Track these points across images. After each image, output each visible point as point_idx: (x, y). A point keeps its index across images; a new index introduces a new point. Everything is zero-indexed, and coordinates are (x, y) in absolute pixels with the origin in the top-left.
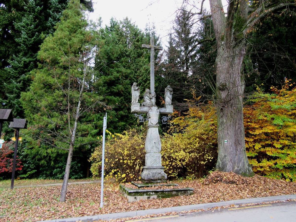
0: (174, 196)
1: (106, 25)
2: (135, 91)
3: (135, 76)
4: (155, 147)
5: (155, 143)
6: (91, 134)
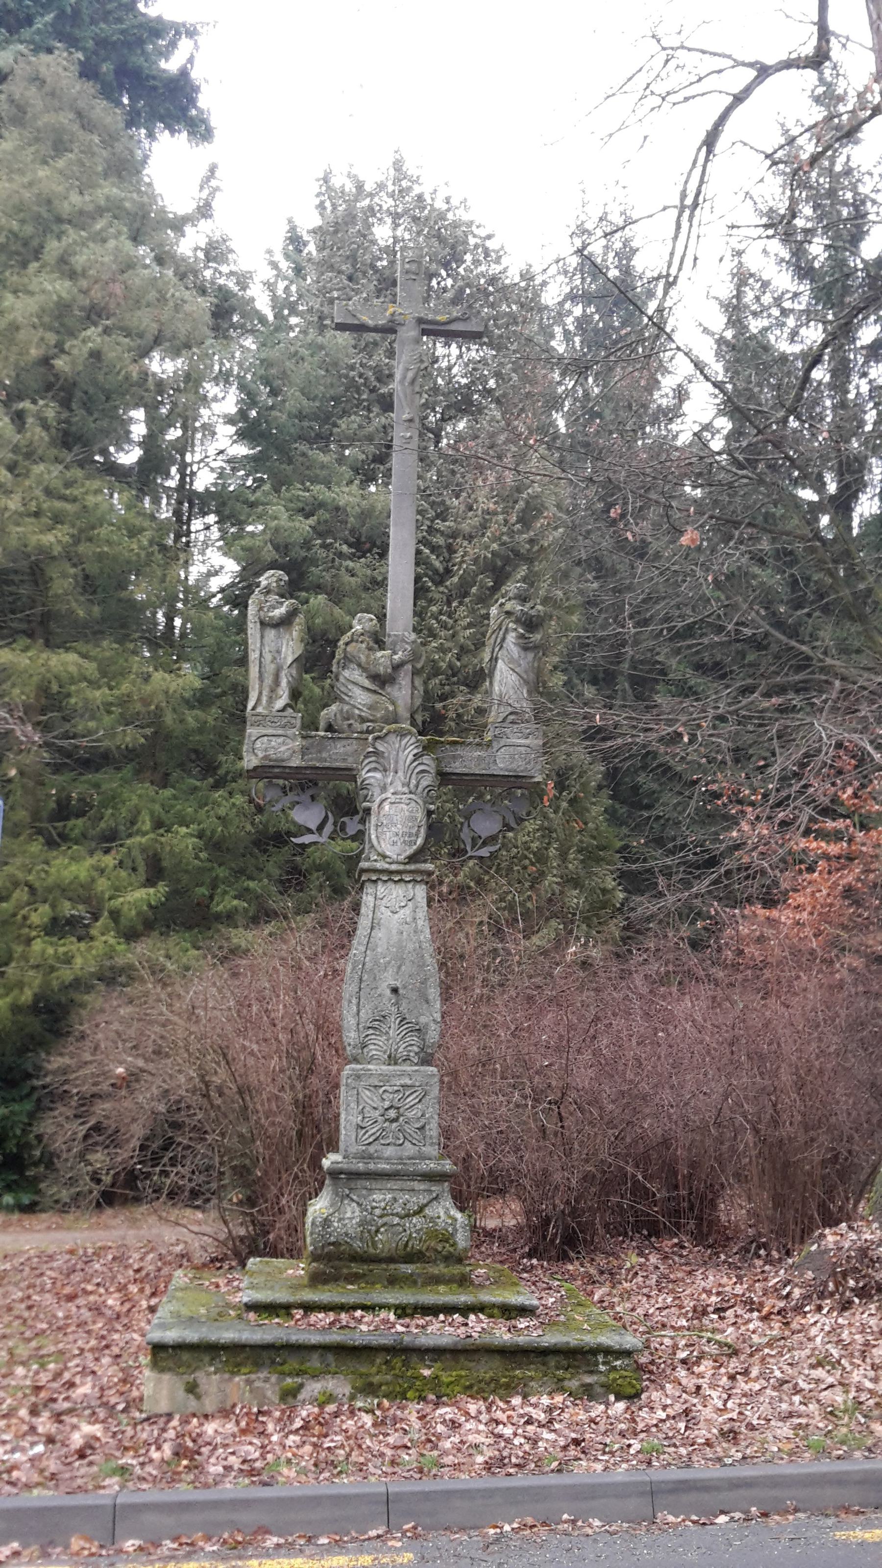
0: (481, 1391)
1: (290, 221)
2: (271, 634)
3: (440, 540)
4: (393, 1021)
5: (395, 990)
6: (115, 915)
